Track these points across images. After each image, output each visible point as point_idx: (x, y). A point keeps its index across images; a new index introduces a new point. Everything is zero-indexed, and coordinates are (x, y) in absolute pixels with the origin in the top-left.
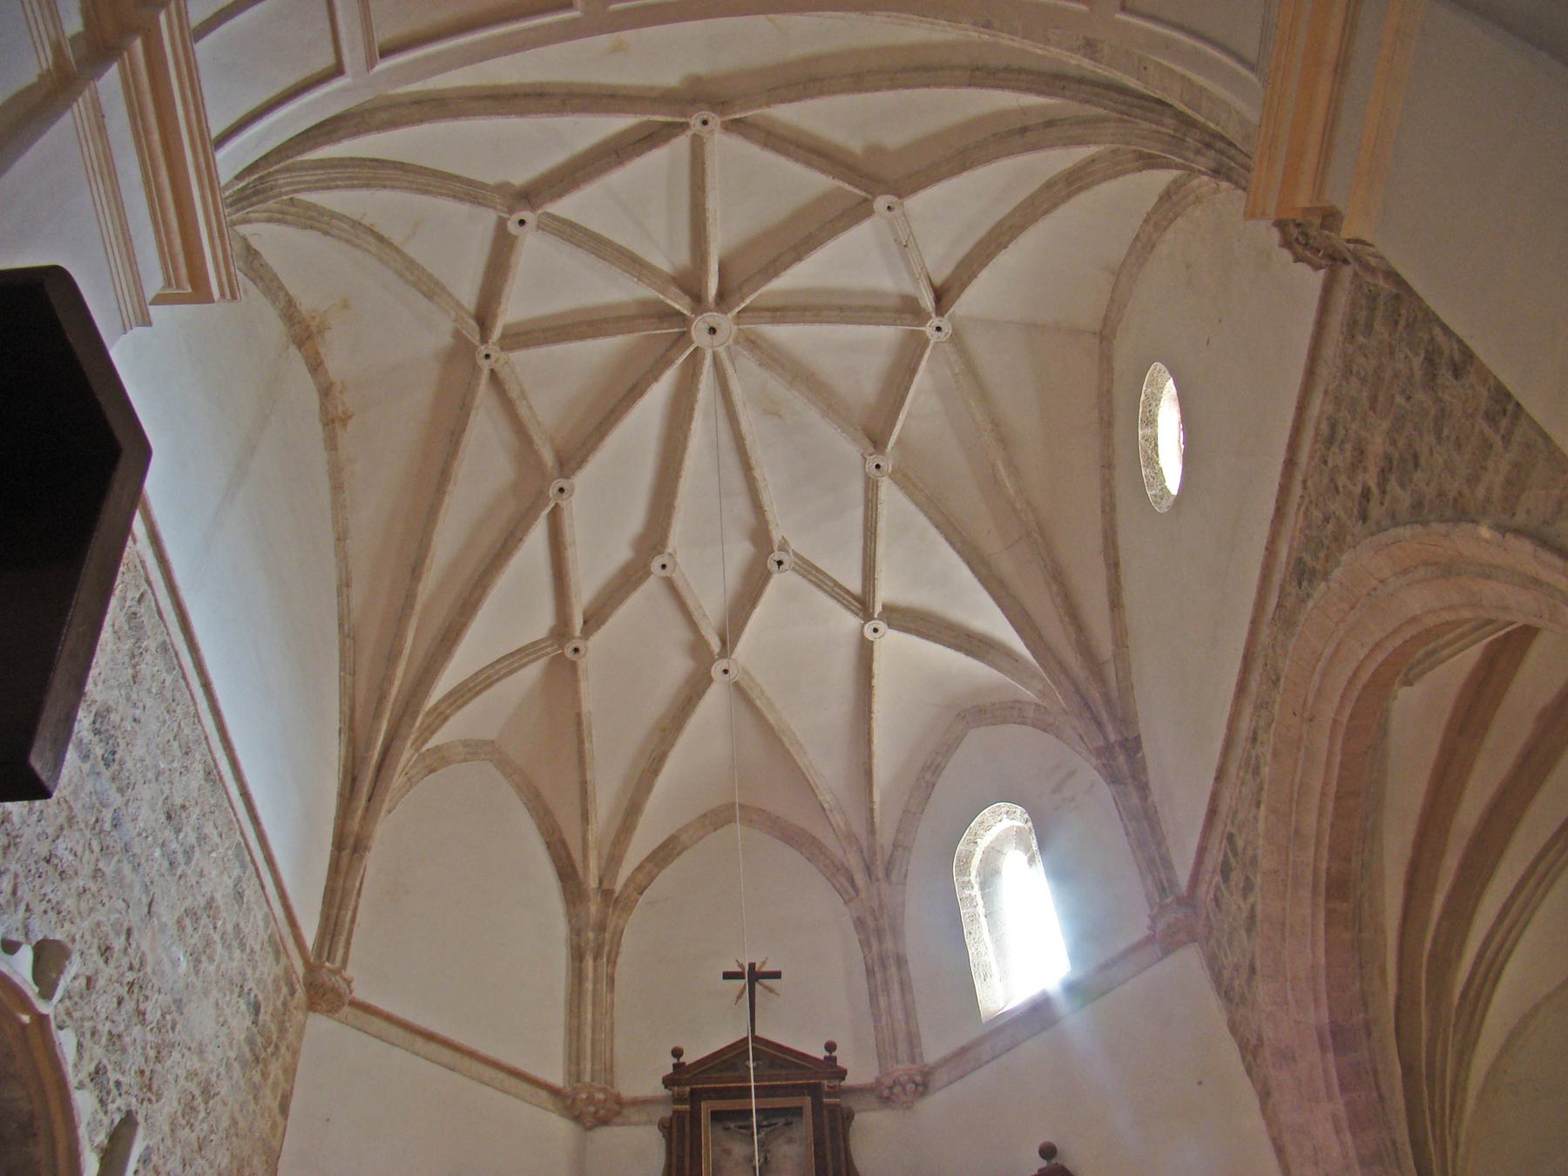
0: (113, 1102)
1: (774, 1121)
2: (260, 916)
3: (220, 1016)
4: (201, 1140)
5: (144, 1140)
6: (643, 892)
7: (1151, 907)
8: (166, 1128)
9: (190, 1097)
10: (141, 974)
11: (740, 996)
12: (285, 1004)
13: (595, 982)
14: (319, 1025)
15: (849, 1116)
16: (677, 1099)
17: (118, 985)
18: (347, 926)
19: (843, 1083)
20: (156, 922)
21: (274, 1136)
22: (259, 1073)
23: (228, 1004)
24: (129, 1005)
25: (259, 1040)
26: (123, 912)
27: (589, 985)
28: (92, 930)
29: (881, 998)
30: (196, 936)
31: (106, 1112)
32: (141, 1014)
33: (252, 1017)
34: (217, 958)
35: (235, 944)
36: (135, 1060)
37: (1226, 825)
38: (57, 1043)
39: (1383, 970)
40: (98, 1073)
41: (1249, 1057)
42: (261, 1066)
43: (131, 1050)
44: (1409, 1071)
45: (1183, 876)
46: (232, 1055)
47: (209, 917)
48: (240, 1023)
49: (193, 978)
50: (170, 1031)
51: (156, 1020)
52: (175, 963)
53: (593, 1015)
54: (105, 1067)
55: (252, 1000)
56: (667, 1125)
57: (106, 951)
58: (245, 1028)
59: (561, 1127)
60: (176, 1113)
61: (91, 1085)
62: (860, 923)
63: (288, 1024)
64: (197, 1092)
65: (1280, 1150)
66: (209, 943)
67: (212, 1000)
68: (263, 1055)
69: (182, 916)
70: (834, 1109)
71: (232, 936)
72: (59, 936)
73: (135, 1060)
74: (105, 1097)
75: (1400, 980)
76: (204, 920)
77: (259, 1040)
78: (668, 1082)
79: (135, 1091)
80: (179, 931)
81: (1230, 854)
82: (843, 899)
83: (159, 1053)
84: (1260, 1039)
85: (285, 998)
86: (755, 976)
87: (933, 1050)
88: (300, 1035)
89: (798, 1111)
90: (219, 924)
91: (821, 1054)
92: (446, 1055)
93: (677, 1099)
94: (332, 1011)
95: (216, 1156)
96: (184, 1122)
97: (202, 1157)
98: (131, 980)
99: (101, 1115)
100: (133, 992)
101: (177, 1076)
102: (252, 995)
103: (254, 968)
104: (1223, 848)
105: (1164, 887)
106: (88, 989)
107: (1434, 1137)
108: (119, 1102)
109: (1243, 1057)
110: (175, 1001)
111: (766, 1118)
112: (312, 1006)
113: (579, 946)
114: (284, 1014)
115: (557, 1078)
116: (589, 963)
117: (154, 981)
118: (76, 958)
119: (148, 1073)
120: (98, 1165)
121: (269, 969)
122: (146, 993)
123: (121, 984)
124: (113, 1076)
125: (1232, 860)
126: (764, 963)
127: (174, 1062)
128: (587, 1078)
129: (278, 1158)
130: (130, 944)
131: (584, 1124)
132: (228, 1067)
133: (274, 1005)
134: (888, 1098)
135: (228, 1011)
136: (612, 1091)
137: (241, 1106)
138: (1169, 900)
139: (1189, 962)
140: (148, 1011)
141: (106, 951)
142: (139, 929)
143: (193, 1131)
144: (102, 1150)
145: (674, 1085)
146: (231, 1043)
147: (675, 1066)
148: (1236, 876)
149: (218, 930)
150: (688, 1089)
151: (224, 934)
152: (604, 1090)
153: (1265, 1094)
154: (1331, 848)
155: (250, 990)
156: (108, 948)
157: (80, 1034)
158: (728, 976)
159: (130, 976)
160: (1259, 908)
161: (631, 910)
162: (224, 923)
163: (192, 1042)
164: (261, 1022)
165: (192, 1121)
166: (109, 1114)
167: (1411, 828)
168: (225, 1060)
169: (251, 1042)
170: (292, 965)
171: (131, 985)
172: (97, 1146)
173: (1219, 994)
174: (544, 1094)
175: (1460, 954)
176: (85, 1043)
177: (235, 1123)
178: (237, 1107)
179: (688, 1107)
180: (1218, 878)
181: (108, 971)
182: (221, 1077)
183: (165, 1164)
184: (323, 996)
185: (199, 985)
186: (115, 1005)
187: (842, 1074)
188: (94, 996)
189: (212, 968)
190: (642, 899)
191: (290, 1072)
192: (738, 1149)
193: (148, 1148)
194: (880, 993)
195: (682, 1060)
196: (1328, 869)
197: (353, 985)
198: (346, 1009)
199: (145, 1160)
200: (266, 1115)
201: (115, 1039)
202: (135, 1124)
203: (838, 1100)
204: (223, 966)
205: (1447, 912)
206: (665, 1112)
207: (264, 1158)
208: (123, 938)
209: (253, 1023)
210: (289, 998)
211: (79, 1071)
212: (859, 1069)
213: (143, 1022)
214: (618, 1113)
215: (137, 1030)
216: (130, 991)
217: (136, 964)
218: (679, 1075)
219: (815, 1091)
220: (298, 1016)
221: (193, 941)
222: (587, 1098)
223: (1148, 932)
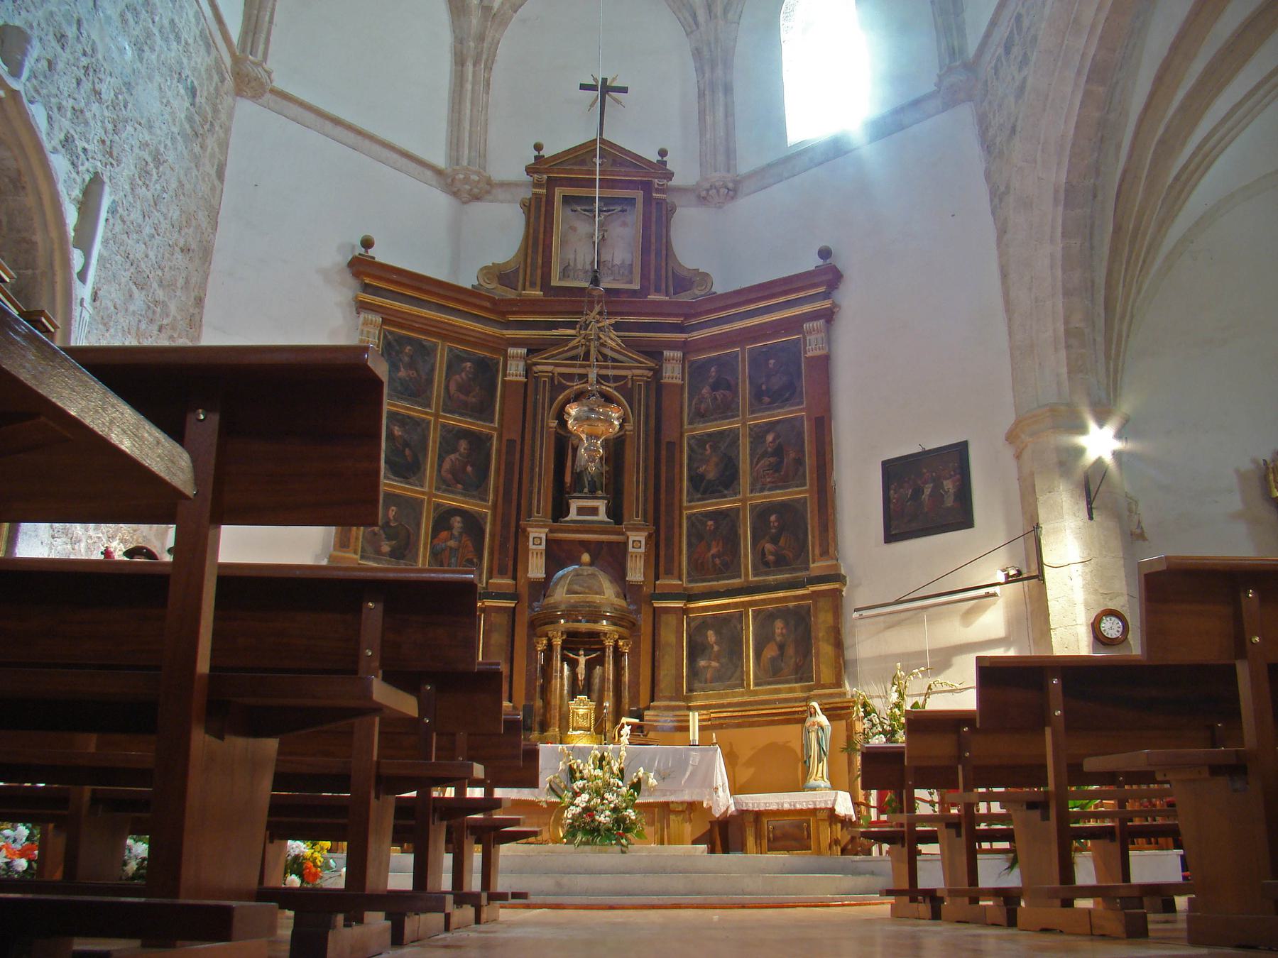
0: (83, 165)
1: (611, 208)
2: (191, 14)
3: (163, 97)
4: (155, 197)
5: (110, 195)
6: (517, 11)
7: (941, 68)
8: (127, 187)
9: (144, 163)
10: (93, 60)
11: (592, 105)
12: (217, 89)
13: (474, 84)
14: (246, 109)
15: (672, 210)
16: (537, 185)
17: (75, 68)
18: (266, 25)
19: (670, 183)
20: (101, 15)
21: (214, 197)
22: (199, 145)
23: (170, 88)
24: (86, 86)
25: (197, 118)
26: (72, 4)
27: (469, 86)
28: (47, 19)
29: (707, 117)
30: (138, 29)
31: (78, 173)
32: (98, 93)
33: (190, 100)
34: (157, 48)
35: (172, 37)
36: (96, 131)
37: (1017, 5)
38: (31, 116)
39: (1119, 146)
40: (67, 141)
41: (996, 201)
42: (200, 139)
43: (92, 123)
44: (1118, 229)
45: (972, 47)
46: (176, 130)
47: (148, 12)
48: (181, 105)
49: (139, 64)
50: (123, 109)
51: (110, 99)
52: (122, 51)
53: (471, 111)
54: (73, 136)
55: (189, 87)
56: (527, 205)
57: (61, 38)
58: (185, 108)
59: (441, 200)
60: (133, 175)
61: (63, 150)
62: (697, 54)
63: (220, 106)
64: (149, 160)
65: (1004, 275)
66: (149, 35)
67: (156, 85)
68: (201, 132)
69: (124, 10)
70: (660, 203)
71: (169, 30)
72: (17, 22)
73: (96, 131)
74: (76, 161)
75: (1130, 156)
76: (144, 15)
77: (197, 118)
78: (530, 170)
79: (99, 156)
80: (122, 23)
81: (1015, 32)
82: (686, 31)
83: (115, 126)
84: (1008, 187)
85: (217, 85)
86: (606, 89)
87: (747, 163)
88: (230, 116)
89: (631, 202)
90: (157, 19)
91: (654, 158)
92: (351, 137)
93: (537, 185)
94: (256, 97)
95: (168, 210)
96: (141, 183)
97: (158, 211)
98: (86, 65)
99: (74, 175)
100: (88, 74)
101: (132, 146)
102: (189, 81)
103: (190, 58)
104: (1011, 25)
105: (953, 53)
106: (50, 71)
107: (1124, 281)
108: (87, 164)
109: (991, 200)
110: (125, 84)
111: (606, 205)
112: (239, 93)
113: (462, 53)
114: (217, 98)
115: (440, 160)
116: (469, 68)
117: (105, 65)
118: (36, 42)
119: (108, 143)
120: (76, 214)
121: (201, 59)
122: (100, 76)
123: (78, 67)
124: (80, 144)
125: (1016, 36)
126: (614, 79)
127: (128, 134)
128: (465, 163)
129: (218, 213)
130: (81, 33)
131: (461, 199)
132: (173, 140)
133: (208, 90)
134: (704, 198)
135: (169, 93)
136: (485, 174)
137: (186, 172)
138: (958, 63)
139: (966, 113)
140: (103, 90)
141: (61, 38)
142: (87, 20)
143: (148, 190)
144: (79, 202)
145: (534, 173)
146: (174, 120)
147: (536, 157)
148: (1016, 50)
149: (156, 24)
150: (545, 176)
151: (161, 28)
152: (479, 174)
153: (1002, 232)
154: (1101, 38)
155: (188, 76)
156: (63, 36)
157: (48, 107)
158: (584, 87)
159: (84, 61)
160: (1030, 81)
161: (506, 25)
162: (161, 18)
163: (142, 118)
164: (197, 104)
165: (147, 182)
166: (80, 175)
167: (1173, 30)
168: (170, 134)
169: (190, 119)
170: (221, 57)
171: (86, 68)
172: (74, 199)
173: (982, 147)
174: (429, 173)
175: (1183, 144)
176: (53, 116)
177: (181, 185)
178: (182, 172)
179: (545, 191)
180: (1001, 51)
181: (65, 56)
182: (168, 147)
183: (129, 215)
184: (248, 84)
185: (143, 71)
186: (75, 85)
187: (670, 176)
188: (56, 77)
189: (154, 57)
190: (516, 16)
191: (224, 145)
192: (582, 227)
193: (114, 201)
194: (707, 112)
195: (542, 153)
196: (1094, 55)
197: (274, 76)
198: (268, 96)
199: (113, 211)
200: (206, 179)
201: (78, 113)
202: (103, 183)
203: (664, 196)
204: (163, 57)
205: (1183, 108)
206: (527, 194)
207: (207, 213)
208: (74, 28)
209: (191, 105)
210: (219, 84)
211: (52, 139)
212: (684, 171)
213: (100, 100)
214: (488, 192)
215: (95, 107)
216: (86, 74)
217: (89, 51)
218: (539, 165)
219: (647, 187)
220: (229, 100)
221: (136, 33)
222: (464, 178)
223: (935, 88)
